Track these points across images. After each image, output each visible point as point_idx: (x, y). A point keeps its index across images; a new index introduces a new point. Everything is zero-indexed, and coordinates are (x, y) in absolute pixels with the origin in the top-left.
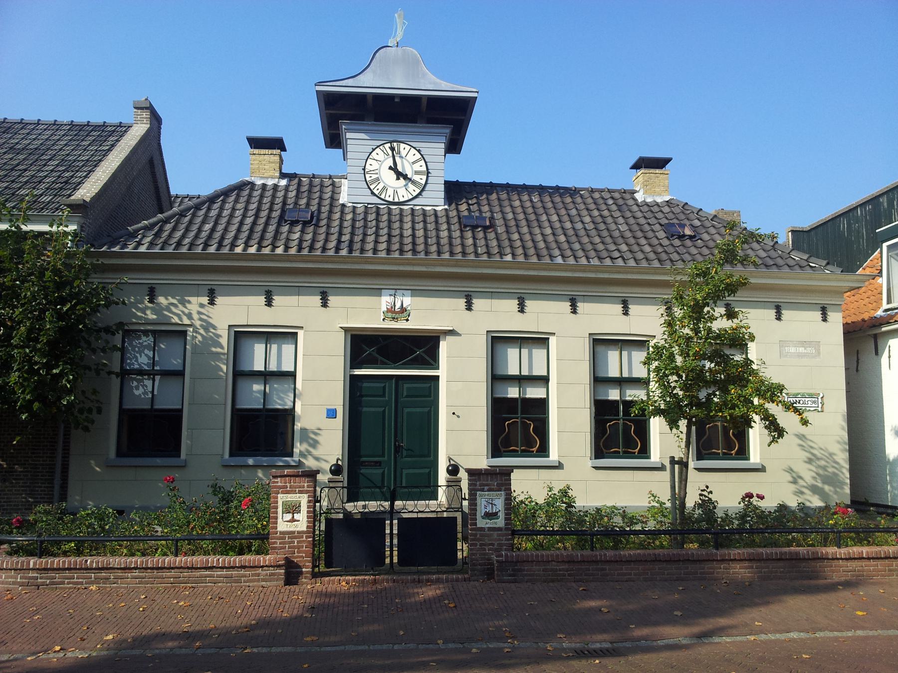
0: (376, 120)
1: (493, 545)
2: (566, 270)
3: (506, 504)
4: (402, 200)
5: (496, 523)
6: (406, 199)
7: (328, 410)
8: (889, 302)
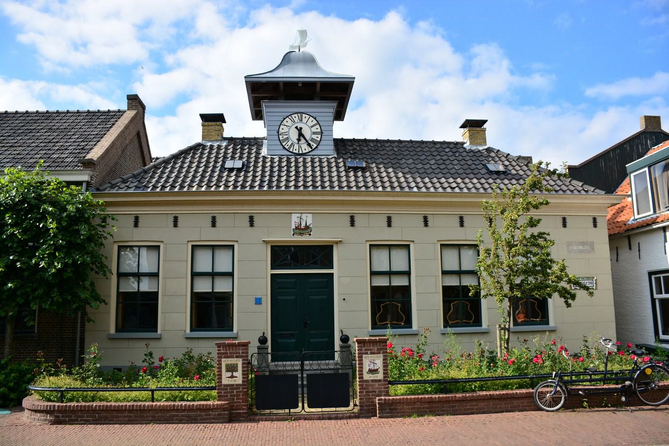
0: (286, 100)
1: (375, 392)
2: (420, 196)
3: (384, 363)
4: (304, 152)
5: (235, 381)
6: (307, 151)
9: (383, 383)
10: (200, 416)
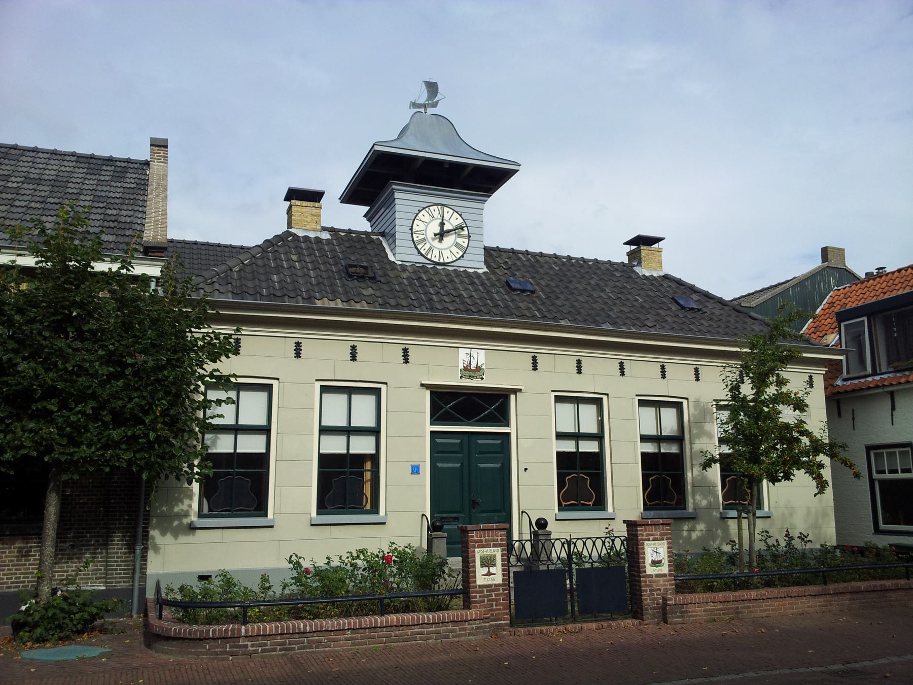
4: (447, 261)
5: (493, 580)
7: (413, 467)
8: (848, 372)
9: (668, 578)
10: (453, 631)
